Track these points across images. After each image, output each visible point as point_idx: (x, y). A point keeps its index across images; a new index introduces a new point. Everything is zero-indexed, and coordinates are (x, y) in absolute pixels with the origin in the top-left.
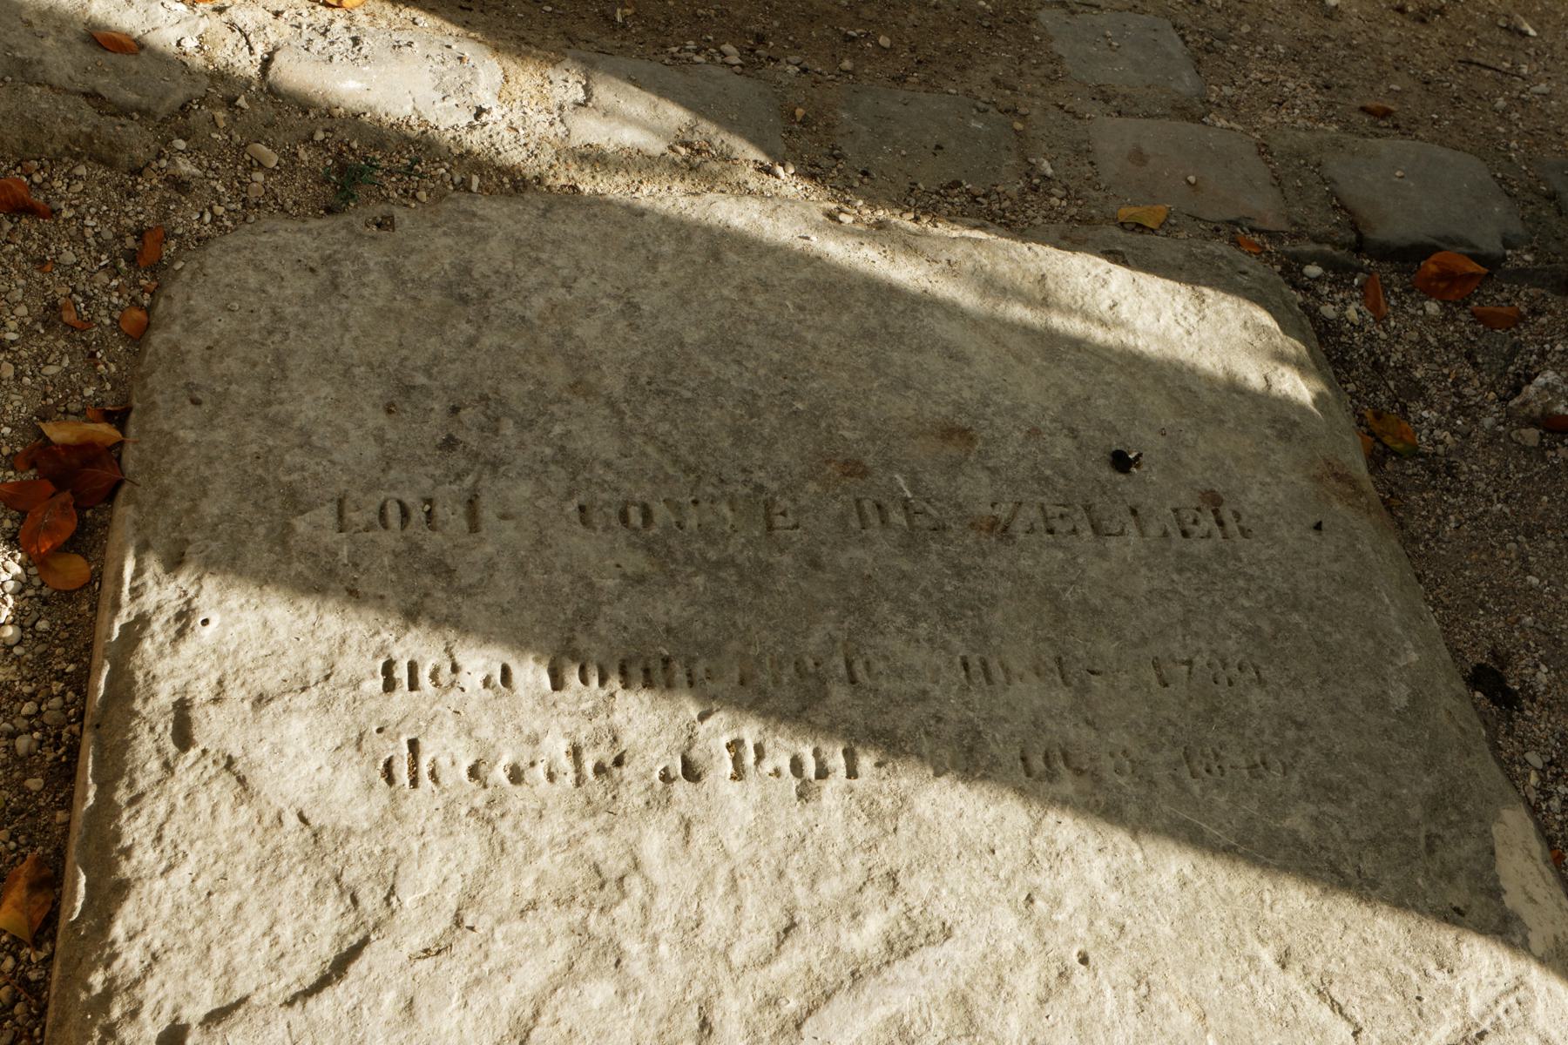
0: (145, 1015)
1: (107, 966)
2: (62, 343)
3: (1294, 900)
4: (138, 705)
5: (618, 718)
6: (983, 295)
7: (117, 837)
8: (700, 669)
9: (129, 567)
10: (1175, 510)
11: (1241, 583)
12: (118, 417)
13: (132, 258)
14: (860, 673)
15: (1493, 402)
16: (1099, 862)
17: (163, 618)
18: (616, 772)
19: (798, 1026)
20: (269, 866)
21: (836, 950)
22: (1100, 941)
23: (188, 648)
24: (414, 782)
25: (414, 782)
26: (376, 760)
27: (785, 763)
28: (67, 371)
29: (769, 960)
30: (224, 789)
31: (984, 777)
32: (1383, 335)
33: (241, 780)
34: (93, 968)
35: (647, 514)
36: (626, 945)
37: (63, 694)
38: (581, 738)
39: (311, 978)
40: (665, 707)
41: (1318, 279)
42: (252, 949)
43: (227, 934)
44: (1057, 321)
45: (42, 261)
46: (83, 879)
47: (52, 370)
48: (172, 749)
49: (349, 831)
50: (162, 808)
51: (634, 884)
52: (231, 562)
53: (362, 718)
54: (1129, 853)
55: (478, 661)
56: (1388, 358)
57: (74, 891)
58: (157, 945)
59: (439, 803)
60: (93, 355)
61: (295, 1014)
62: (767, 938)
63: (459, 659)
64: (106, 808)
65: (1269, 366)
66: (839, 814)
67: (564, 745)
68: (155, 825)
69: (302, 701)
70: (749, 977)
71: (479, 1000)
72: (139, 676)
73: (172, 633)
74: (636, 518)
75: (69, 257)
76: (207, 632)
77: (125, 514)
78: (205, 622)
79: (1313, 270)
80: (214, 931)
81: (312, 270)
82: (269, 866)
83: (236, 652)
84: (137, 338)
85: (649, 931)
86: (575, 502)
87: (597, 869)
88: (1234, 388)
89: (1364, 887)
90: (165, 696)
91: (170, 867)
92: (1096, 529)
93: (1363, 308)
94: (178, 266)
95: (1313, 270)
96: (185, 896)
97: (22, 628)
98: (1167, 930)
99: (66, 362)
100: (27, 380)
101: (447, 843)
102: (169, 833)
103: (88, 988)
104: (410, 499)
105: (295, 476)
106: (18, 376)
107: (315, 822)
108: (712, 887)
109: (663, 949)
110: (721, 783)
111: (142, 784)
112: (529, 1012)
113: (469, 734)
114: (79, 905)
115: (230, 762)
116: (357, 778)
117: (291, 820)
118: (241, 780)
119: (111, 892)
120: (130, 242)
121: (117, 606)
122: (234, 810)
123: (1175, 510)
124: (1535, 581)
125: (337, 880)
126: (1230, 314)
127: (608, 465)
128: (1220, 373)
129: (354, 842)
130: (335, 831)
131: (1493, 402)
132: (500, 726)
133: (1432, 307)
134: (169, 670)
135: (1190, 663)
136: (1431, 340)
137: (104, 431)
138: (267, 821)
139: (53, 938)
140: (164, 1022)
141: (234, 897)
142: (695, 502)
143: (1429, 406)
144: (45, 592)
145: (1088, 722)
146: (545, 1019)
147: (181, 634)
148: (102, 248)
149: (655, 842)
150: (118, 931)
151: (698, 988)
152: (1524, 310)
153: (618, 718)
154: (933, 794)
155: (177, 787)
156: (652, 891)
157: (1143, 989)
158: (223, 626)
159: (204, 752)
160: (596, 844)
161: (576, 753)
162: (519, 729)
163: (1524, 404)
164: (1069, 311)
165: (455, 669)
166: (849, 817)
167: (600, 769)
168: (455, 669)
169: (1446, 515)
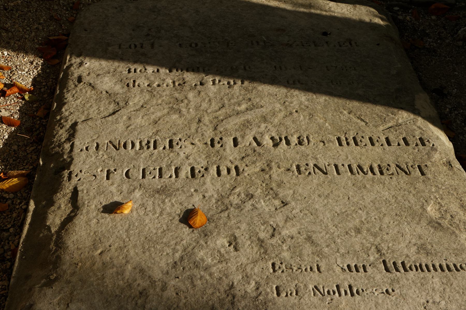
0: (69, 121)
1: (61, 115)
2: (54, 23)
3: (356, 104)
4: (69, 77)
5: (185, 76)
6: (293, 7)
7: (64, 96)
8: (206, 69)
9: (68, 58)
10: (339, 42)
11: (354, 54)
12: (68, 35)
13: (71, 8)
14: (247, 68)
15: (449, 37)
16: (305, 97)
17: (76, 64)
18: (183, 85)
19: (222, 121)
20: (99, 100)
21: (233, 110)
22: (301, 109)
23: (81, 69)
24: (134, 86)
25: (134, 86)
26: (125, 83)
27: (226, 83)
28: (55, 28)
29: (217, 111)
30: (89, 89)
31: (276, 84)
32: (418, 23)
33: (93, 87)
34: (58, 116)
35: (196, 45)
36: (182, 109)
37: (52, 81)
38: (176, 79)
39: (107, 115)
40: (197, 75)
41: (398, 10)
42: (94, 111)
43: (88, 109)
44: (313, 11)
45: (50, 9)
46: (56, 104)
47: (52, 28)
48: (77, 83)
49: (118, 94)
50: (74, 92)
51: (186, 101)
52: (93, 55)
53: (122, 77)
54: (312, 96)
55: (150, 69)
56: (419, 28)
57: (54, 106)
58: (72, 111)
59: (140, 90)
60: (61, 25)
61: (103, 120)
62: (217, 108)
63: (147, 68)
64: (62, 93)
65: (372, 18)
66: (238, 90)
67: (171, 81)
68: (72, 94)
69: (108, 75)
70: (211, 114)
71: (146, 118)
72: (70, 73)
73: (78, 66)
74: (193, 45)
75: (56, 7)
76: (86, 65)
77: (68, 49)
78: (86, 64)
79: (396, 8)
80: (85, 109)
81: (116, 8)
82: (99, 100)
83: (93, 69)
84: (72, 22)
85: (188, 107)
86: (179, 43)
87: (177, 99)
88: (361, 22)
89: (375, 102)
90: (76, 75)
91: (76, 100)
92: (315, 45)
93: (412, 17)
94: (83, 9)
95: (396, 8)
96: (79, 104)
97: (43, 71)
98: (320, 107)
99: (55, 26)
100: (45, 30)
101: (141, 95)
102: (76, 95)
103: (56, 119)
104: (137, 43)
105: (109, 41)
106: (43, 29)
107: (110, 93)
108: (204, 101)
109: (191, 110)
110: (209, 86)
111: (70, 89)
112: (157, 119)
113: (148, 79)
114: (55, 107)
115: (90, 84)
116: (120, 86)
117: (104, 93)
118: (93, 87)
119: (62, 104)
120: (71, 5)
121: (65, 63)
122: (91, 92)
123: (339, 42)
124: (457, 73)
125: (114, 101)
126: (363, 9)
127: (187, 37)
128: (358, 19)
129: (118, 95)
130: (114, 94)
131: (449, 37)
132: (156, 78)
133: (434, 17)
134: (76, 72)
135: (336, 67)
136: (433, 24)
137: (64, 38)
138: (98, 93)
139: (48, 118)
140: (73, 122)
141: (90, 104)
142: (209, 43)
143: (430, 38)
144: (49, 66)
145: (306, 76)
146: (161, 120)
147: (80, 66)
148: (64, 6)
149: (191, 95)
150: (63, 110)
151: (199, 116)
152: (461, 16)
153: (185, 76)
154: (263, 87)
155: (78, 89)
156: (189, 101)
157: (311, 116)
158: (90, 65)
159: (85, 83)
160: (177, 95)
161: (174, 82)
162: (160, 78)
163: (458, 36)
164: (317, 9)
165: (146, 69)
166: (240, 90)
167: (179, 85)
168: (146, 69)
169: (432, 61)
